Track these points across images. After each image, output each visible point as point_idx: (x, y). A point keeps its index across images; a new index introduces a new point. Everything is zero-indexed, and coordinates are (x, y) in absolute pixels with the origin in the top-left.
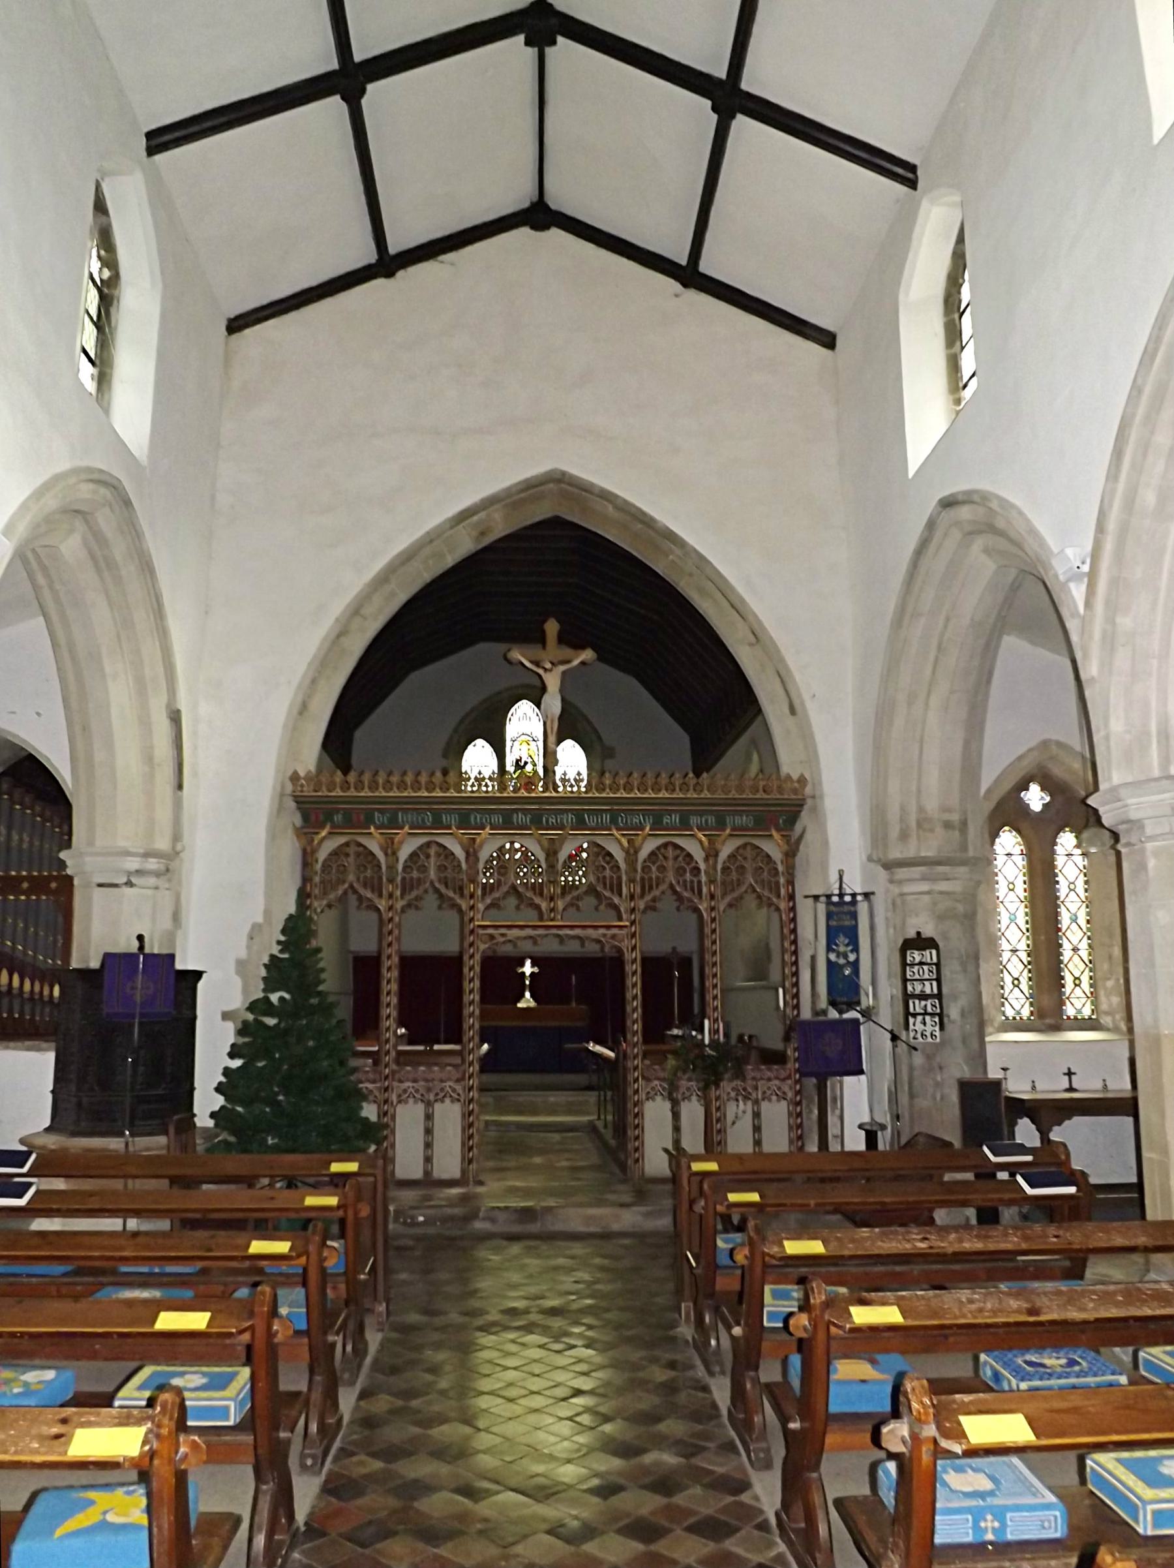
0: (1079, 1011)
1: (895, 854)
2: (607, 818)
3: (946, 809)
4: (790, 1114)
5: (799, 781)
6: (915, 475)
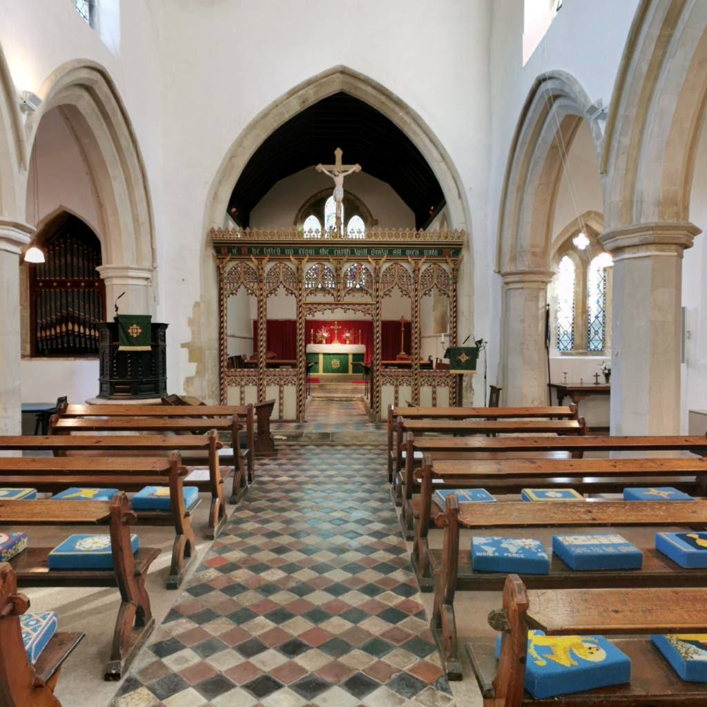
0: (596, 347)
1: (507, 268)
2: (366, 251)
3: (532, 246)
4: (450, 392)
5: (461, 233)
6: (527, 64)
